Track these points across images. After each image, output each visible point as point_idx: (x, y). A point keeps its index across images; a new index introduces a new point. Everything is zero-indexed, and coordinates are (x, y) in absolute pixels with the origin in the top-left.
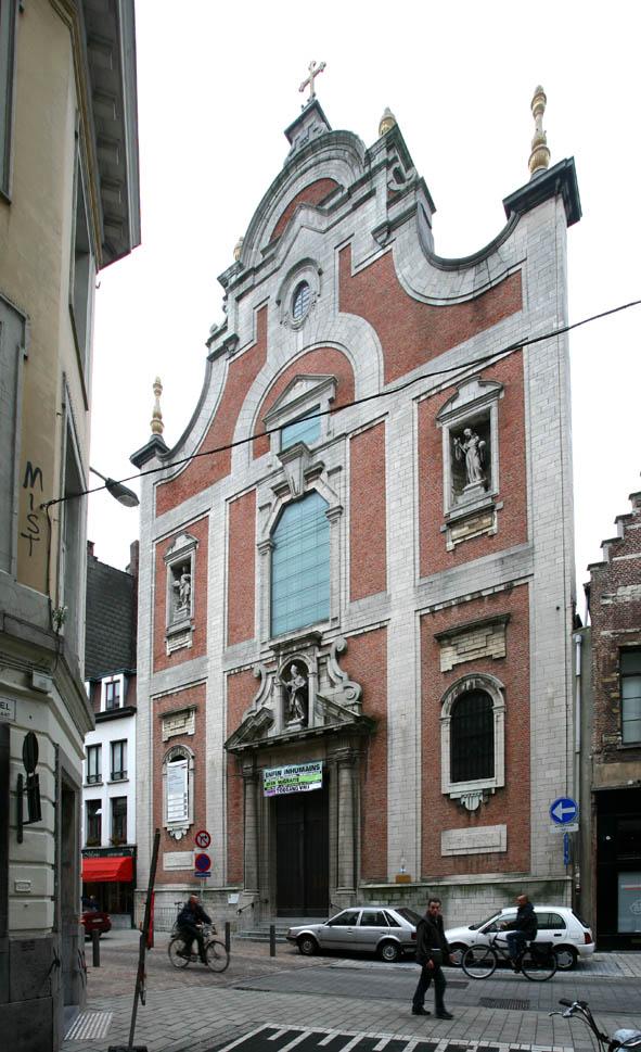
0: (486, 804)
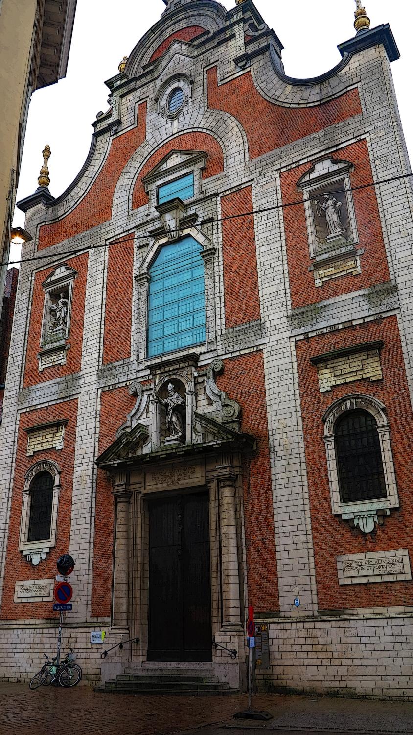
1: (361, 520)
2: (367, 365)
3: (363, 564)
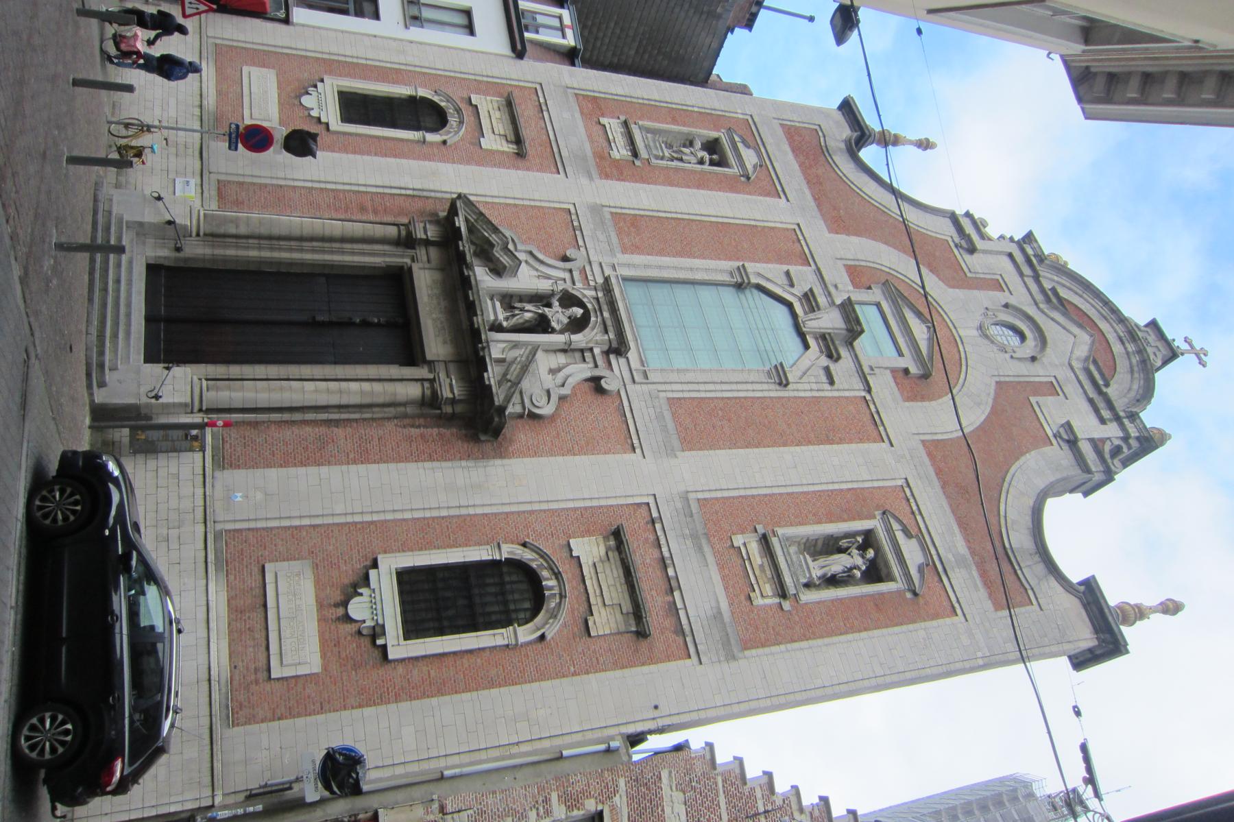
3: (298, 602)
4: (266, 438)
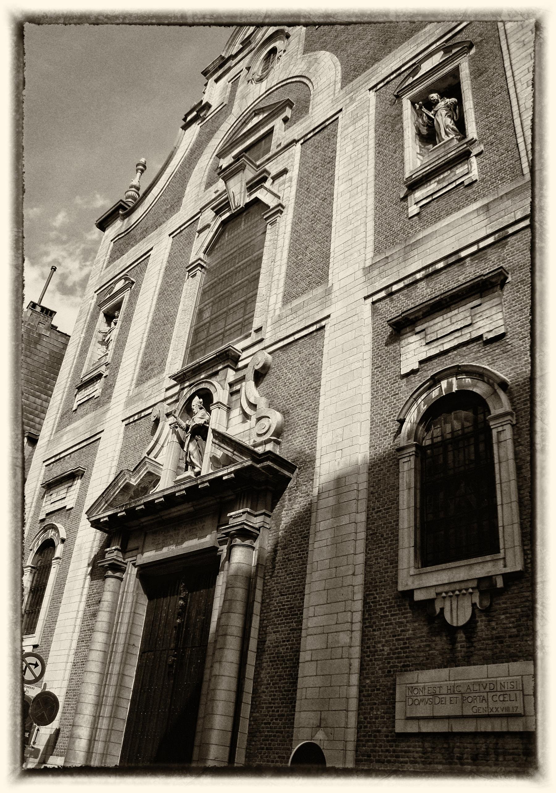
0: (487, 611)
1: (447, 604)
2: (481, 314)
3: (444, 691)
4: (265, 724)
